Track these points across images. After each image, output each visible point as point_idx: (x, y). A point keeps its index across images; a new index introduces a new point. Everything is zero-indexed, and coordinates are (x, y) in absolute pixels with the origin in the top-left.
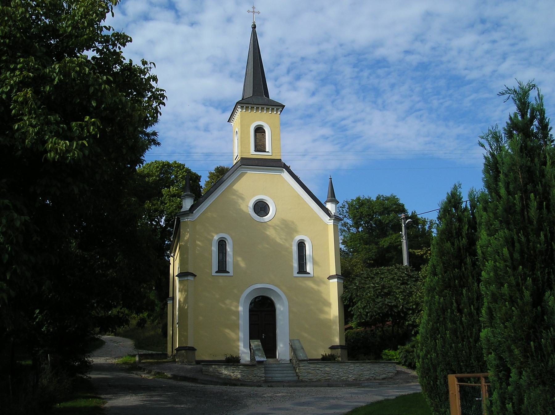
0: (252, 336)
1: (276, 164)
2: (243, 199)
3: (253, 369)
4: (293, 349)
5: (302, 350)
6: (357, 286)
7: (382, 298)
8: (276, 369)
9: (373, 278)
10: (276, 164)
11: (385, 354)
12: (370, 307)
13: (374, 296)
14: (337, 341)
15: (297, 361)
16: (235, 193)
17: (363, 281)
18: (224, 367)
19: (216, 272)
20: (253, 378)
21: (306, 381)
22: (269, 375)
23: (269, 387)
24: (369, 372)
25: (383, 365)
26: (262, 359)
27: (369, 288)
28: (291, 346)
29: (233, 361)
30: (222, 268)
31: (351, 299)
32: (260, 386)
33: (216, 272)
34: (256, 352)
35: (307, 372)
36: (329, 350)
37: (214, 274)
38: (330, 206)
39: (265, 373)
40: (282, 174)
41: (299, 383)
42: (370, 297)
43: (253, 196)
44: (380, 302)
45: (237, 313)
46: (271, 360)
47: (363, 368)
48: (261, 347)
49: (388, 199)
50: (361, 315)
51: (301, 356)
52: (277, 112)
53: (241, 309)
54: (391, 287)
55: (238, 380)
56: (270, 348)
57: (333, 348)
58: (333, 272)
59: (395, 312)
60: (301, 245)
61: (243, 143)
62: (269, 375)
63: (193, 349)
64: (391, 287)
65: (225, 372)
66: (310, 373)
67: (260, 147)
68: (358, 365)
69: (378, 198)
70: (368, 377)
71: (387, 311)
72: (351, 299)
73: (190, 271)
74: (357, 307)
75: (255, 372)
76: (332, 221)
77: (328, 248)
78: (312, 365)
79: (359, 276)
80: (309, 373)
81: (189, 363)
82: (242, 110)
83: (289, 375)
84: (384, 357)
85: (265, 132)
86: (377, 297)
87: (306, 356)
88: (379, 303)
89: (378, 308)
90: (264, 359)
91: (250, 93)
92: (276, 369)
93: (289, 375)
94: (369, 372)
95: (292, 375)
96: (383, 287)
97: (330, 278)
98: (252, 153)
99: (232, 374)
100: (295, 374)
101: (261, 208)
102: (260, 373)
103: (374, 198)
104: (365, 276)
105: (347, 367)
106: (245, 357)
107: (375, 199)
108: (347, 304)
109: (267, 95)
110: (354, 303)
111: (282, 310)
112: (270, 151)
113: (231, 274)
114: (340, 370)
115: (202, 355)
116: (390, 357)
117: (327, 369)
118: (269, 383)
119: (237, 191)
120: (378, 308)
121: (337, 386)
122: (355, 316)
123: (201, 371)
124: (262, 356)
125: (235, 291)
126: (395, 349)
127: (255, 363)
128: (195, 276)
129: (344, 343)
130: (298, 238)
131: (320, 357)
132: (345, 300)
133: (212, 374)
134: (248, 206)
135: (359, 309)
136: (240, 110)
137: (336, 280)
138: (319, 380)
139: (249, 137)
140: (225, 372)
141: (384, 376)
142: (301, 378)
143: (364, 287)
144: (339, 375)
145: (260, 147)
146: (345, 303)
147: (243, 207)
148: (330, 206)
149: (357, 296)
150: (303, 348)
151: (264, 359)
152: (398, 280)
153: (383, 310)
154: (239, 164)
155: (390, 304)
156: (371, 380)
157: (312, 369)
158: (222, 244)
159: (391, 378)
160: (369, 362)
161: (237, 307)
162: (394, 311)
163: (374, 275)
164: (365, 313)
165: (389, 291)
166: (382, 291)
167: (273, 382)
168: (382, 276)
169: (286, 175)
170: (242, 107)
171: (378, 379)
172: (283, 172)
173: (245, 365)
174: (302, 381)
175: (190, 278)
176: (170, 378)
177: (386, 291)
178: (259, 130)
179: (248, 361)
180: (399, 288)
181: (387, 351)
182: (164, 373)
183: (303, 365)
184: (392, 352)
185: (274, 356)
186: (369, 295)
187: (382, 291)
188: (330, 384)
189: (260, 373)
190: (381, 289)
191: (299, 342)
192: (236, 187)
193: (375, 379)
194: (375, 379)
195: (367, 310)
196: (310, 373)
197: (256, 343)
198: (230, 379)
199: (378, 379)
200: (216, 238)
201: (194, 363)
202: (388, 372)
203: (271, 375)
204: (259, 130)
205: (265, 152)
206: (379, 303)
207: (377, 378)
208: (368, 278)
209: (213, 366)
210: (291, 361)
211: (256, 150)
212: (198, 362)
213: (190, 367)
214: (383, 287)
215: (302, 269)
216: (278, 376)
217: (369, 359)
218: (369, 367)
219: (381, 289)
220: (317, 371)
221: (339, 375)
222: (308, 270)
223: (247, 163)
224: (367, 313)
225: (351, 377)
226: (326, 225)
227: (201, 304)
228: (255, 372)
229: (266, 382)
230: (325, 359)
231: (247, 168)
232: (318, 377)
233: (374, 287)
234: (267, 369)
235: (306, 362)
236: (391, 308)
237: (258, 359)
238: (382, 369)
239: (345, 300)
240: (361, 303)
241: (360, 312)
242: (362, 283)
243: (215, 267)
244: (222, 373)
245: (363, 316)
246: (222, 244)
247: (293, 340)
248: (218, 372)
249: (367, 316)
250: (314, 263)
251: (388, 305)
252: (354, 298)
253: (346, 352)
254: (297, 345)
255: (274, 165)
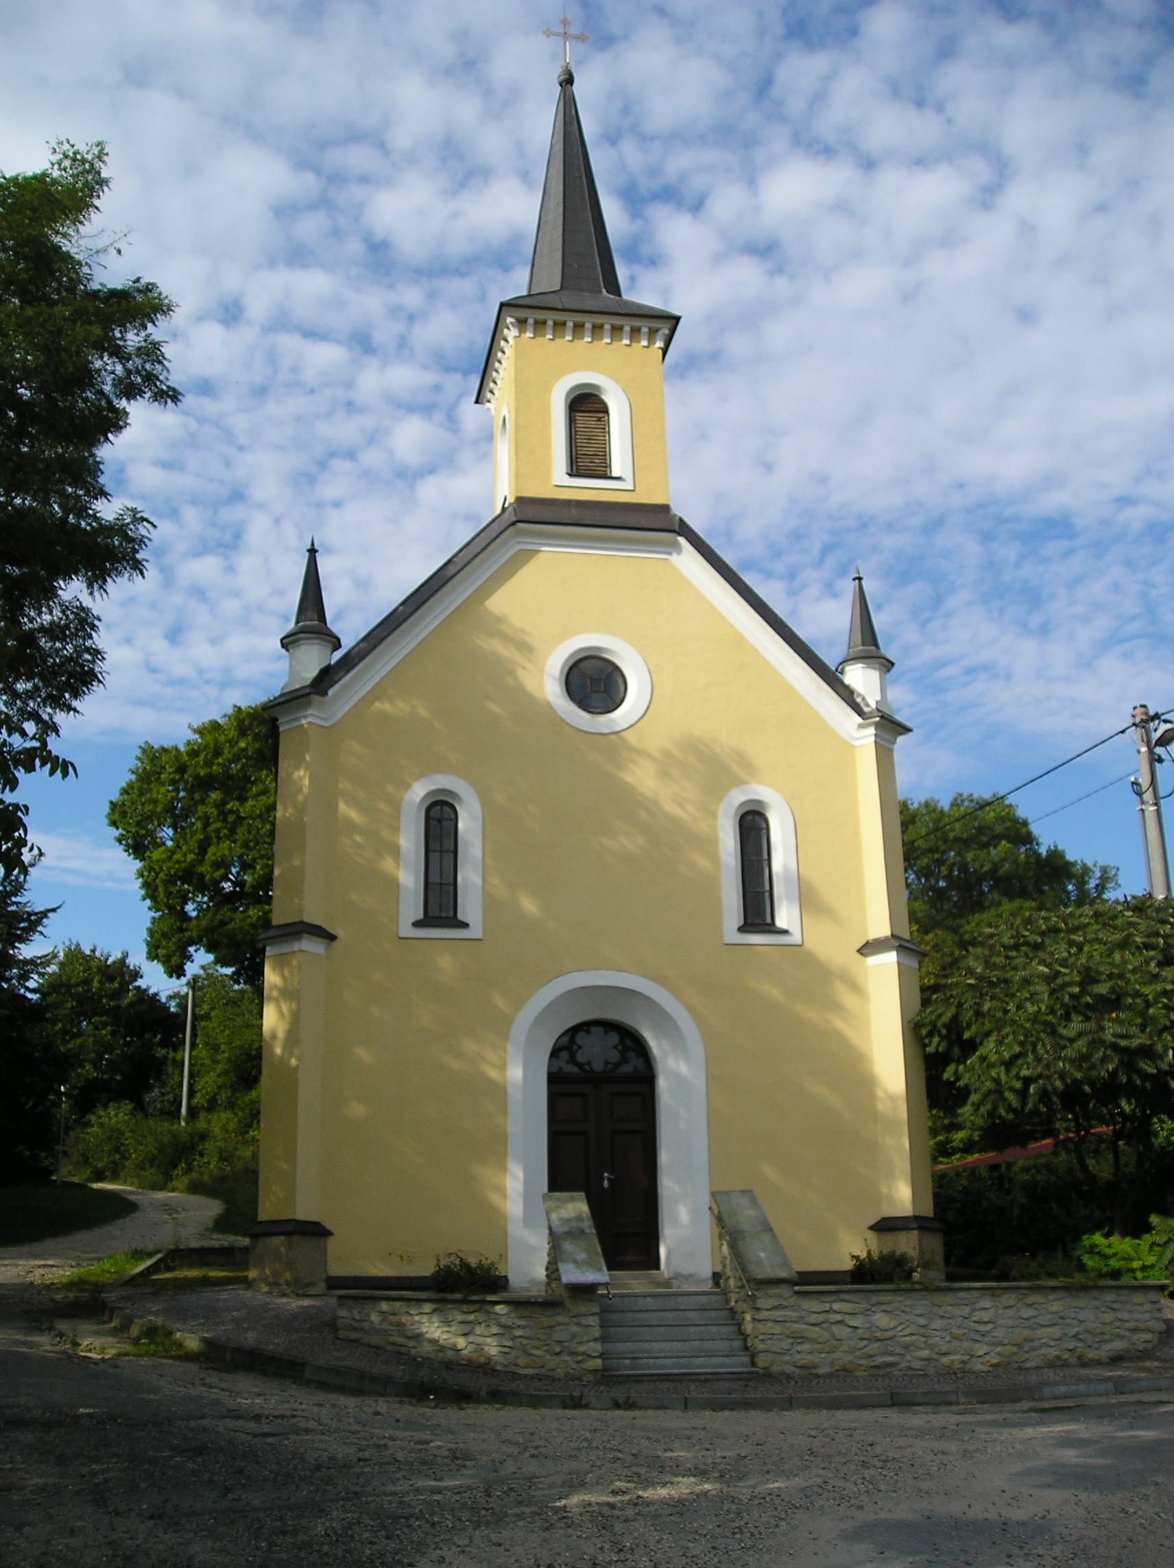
0: (561, 1178)
1: (653, 523)
2: (525, 647)
3: (546, 1321)
4: (728, 1230)
5: (766, 1237)
6: (980, 978)
7: (1088, 1019)
8: (653, 1318)
9: (1037, 947)
10: (653, 523)
11: (1092, 1250)
12: (1039, 1060)
13: (1052, 1011)
14: (902, 1196)
15: (745, 1281)
16: (495, 626)
17: (1000, 960)
18: (427, 1307)
19: (417, 924)
20: (552, 1362)
21: (788, 1377)
22: (621, 1347)
23: (617, 1406)
24: (1055, 1332)
25: (1110, 1297)
26: (590, 1277)
27: (1026, 982)
28: (719, 1219)
29: (468, 1284)
30: (441, 908)
31: (955, 1027)
32: (577, 1403)
33: (417, 924)
34: (567, 1246)
35: (789, 1334)
36: (872, 1237)
37: (406, 930)
38: (859, 677)
39: (603, 1339)
40: (674, 559)
41: (757, 1386)
42: (1034, 1019)
43: (565, 636)
44: (1080, 1034)
45: (498, 1092)
46: (635, 1282)
47: (1030, 1313)
48: (588, 1225)
49: (983, 805)
50: (999, 1092)
51: (764, 1261)
52: (651, 341)
53: (515, 1073)
54: (1121, 976)
55: (482, 1368)
56: (627, 1226)
57: (885, 1226)
58: (879, 923)
59: (1146, 1077)
60: (752, 825)
61: (528, 454)
62: (621, 1347)
63: (316, 1231)
64: (1121, 976)
65: (435, 1329)
66: (804, 1339)
67: (587, 458)
68: (1009, 1299)
69: (955, 804)
70: (1053, 1352)
71: (1115, 1071)
72: (955, 1027)
73: (313, 916)
74: (983, 1059)
75: (560, 1334)
76: (872, 730)
77: (856, 834)
78: (813, 1305)
79: (982, 944)
80: (800, 1338)
81: (300, 1287)
82: (522, 331)
83: (709, 1345)
84: (1090, 1262)
85: (605, 410)
86: (1067, 1018)
87: (786, 1264)
88: (1072, 1041)
89: (1072, 1061)
90: (597, 1275)
91: (551, 280)
92: (653, 1318)
93: (709, 1345)
94: (1055, 1332)
95: (722, 1345)
96: (1089, 977)
97: (869, 948)
98: (557, 480)
99: (461, 1342)
100: (737, 1344)
101: (594, 682)
102: (582, 1337)
103: (945, 804)
104: (1006, 940)
105: (966, 1311)
106: (528, 1264)
107: (946, 808)
108: (938, 1050)
109: (614, 288)
110: (970, 1047)
111: (679, 1073)
112: (628, 476)
113: (476, 931)
114: (938, 1324)
115: (352, 1255)
116: (1113, 1263)
117: (882, 1320)
118: (618, 1386)
119: (500, 620)
120: (1072, 1061)
121: (937, 1401)
122: (974, 1098)
123: (332, 1325)
124: (589, 1264)
125: (499, 1001)
126: (1137, 1228)
127: (561, 1292)
128: (332, 938)
129: (928, 1210)
130: (737, 797)
131: (849, 1265)
132: (930, 1034)
133: (375, 1340)
134: (548, 685)
135: (991, 1066)
136: (511, 333)
137: (891, 957)
138: (845, 1372)
139: (547, 425)
140: (435, 1329)
141: (1118, 1345)
142: (762, 1361)
143: (1006, 981)
144: (931, 1347)
145: (587, 458)
146: (930, 1050)
147: (529, 681)
148: (859, 677)
149: (978, 1014)
150: (768, 1229)
151: (597, 1275)
152: (1147, 947)
153: (1093, 1067)
154: (510, 516)
155: (1123, 1043)
156: (1066, 1365)
157: (814, 1318)
158: (440, 818)
159: (1145, 1355)
160: (1054, 1289)
161: (502, 1068)
162: (1140, 1073)
163: (1042, 934)
164: (1018, 1085)
165: (1112, 990)
166: (1083, 992)
167: (639, 1379)
168: (1078, 938)
169: (687, 560)
170: (521, 323)
171: (1098, 1363)
172: (677, 548)
173: (522, 1305)
174: (767, 1375)
175: (310, 946)
176: (189, 1357)
177: (1102, 989)
178: (586, 405)
179: (534, 1282)
180: (1155, 978)
181: (1097, 1238)
182: (171, 1333)
183: (775, 1302)
184: (1120, 1244)
185: (653, 1262)
186: (1031, 1008)
187: (1083, 992)
188: (898, 1391)
189: (582, 1337)
190: (1081, 984)
191: (754, 1202)
192: (498, 603)
193: (1084, 1363)
194: (1084, 1363)
195: (1025, 1072)
196: (804, 1339)
197: (576, 1207)
198: (449, 1365)
199: (1098, 1363)
200: (418, 792)
201: (321, 1287)
202: (1134, 1330)
203: (629, 1346)
204: (586, 405)
205: (606, 476)
206: (1072, 1041)
207: (1091, 1354)
208: (1016, 947)
209: (385, 1306)
210: (717, 1284)
211: (576, 468)
212: (335, 1283)
213: (295, 1304)
214: (1089, 977)
215: (757, 913)
216: (660, 1353)
217: (1051, 1275)
218: (1056, 1306)
219: (1081, 984)
220: (835, 1329)
221: (931, 1347)
222: (781, 923)
223: (534, 516)
224: (1027, 1081)
225: (985, 1356)
226: (848, 748)
227: (363, 1054)
228: (560, 1334)
229: (606, 1377)
230: (866, 1274)
231: (540, 535)
232: (842, 1357)
233: (1049, 979)
234: (615, 1316)
235: (784, 1291)
236: (1130, 1058)
237: (571, 1274)
238: (1108, 1317)
239: (930, 1034)
240: (1000, 1043)
241: (997, 1081)
242: (996, 967)
243: (411, 906)
244: (418, 1337)
245: (1009, 1095)
246: (440, 818)
247: (727, 1193)
248: (402, 1333)
249: (1023, 1094)
250: (807, 899)
251: (1115, 1047)
252: (969, 1026)
253: (935, 1243)
254: (746, 1216)
255: (643, 523)
